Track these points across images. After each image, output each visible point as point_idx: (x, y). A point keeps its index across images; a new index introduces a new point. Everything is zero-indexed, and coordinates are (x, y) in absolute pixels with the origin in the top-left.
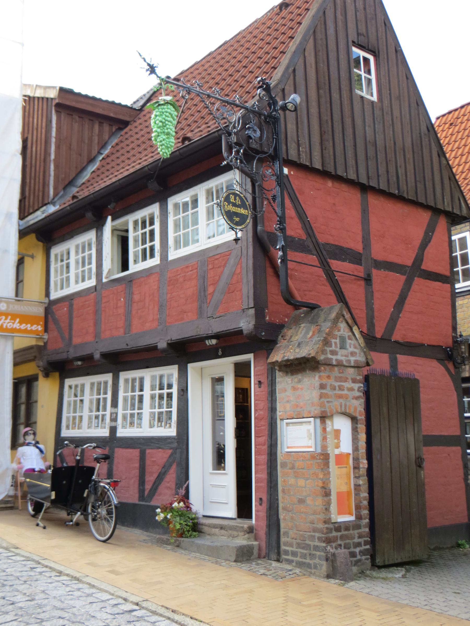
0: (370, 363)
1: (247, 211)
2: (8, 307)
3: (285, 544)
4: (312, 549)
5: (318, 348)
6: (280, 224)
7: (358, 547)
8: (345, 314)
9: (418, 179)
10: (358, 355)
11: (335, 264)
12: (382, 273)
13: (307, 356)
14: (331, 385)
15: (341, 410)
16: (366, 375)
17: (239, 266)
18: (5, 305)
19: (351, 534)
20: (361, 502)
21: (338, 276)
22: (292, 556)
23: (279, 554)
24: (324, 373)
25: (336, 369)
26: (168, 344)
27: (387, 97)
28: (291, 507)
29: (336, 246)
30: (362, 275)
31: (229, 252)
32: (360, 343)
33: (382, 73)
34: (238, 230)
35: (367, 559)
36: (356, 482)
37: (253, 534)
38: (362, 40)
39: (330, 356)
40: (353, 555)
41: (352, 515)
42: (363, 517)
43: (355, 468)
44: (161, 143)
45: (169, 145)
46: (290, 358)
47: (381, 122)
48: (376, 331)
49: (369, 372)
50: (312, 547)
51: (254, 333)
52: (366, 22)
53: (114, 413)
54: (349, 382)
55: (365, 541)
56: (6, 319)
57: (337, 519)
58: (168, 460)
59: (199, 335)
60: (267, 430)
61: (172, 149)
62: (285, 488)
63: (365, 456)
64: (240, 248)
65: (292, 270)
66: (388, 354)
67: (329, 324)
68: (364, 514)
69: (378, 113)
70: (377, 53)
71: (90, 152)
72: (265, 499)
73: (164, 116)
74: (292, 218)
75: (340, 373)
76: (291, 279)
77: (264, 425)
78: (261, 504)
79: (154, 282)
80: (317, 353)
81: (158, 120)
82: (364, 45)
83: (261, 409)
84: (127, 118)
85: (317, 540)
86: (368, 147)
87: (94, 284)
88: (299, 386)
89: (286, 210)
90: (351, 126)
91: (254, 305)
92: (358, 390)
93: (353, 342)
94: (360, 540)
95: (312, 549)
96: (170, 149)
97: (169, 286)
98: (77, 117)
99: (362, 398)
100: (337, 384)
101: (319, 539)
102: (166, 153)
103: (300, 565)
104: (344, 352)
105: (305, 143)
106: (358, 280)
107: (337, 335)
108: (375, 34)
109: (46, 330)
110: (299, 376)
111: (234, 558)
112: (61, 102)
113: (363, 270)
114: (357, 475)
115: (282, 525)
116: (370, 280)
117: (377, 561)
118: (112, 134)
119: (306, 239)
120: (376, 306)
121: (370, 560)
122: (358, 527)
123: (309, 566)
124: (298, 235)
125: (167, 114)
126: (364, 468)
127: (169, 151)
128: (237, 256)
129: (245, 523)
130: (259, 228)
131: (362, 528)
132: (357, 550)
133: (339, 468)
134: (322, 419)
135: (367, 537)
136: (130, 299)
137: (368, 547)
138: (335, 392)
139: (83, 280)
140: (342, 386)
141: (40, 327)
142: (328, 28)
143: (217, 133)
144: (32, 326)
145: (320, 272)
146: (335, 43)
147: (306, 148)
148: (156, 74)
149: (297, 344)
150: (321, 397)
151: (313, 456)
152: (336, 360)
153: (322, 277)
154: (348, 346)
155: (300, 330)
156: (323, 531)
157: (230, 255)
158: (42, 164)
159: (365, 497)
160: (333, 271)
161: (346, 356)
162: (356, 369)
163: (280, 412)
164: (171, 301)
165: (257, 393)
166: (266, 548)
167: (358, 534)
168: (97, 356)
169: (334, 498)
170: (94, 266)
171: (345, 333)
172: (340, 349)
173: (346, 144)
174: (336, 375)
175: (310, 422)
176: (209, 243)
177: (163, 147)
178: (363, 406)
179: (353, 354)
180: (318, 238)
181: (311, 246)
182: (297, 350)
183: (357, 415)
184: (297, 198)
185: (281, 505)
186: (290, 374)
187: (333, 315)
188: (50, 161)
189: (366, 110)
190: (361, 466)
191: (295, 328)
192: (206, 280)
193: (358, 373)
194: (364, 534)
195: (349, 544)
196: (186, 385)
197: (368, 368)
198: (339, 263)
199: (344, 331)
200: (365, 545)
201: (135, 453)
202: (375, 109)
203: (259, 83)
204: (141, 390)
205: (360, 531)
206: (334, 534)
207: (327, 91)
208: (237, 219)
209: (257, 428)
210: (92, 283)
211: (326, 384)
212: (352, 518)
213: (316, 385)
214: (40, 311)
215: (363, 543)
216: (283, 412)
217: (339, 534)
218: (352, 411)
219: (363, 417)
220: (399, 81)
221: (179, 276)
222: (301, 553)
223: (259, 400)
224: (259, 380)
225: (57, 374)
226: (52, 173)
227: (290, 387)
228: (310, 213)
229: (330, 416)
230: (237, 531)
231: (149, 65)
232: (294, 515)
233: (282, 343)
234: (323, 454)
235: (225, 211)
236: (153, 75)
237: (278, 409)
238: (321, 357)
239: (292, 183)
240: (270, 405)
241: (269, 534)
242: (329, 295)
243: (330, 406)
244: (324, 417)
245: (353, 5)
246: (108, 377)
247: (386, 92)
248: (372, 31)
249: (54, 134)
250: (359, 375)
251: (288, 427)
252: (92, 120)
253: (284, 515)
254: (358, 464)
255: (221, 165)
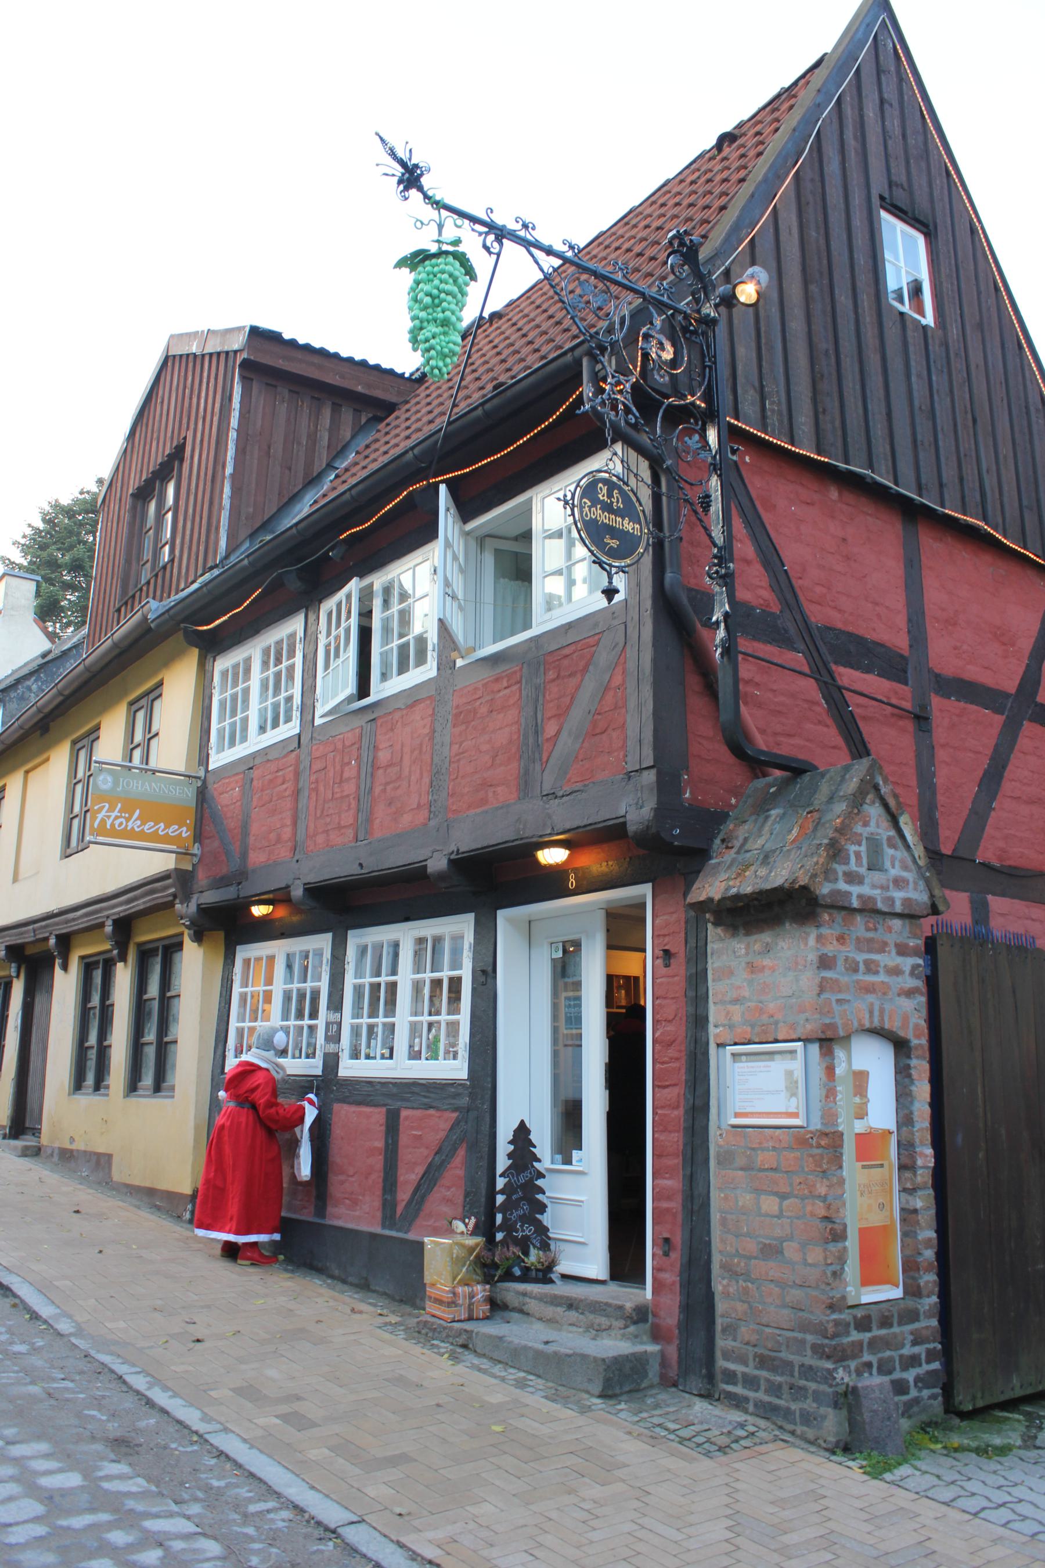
0: (941, 908)
1: (637, 526)
2: (116, 783)
3: (727, 1356)
4: (796, 1374)
5: (817, 863)
6: (719, 565)
7: (913, 1367)
8: (881, 783)
9: (1025, 502)
10: (911, 885)
11: (847, 676)
12: (953, 705)
13: (787, 885)
14: (847, 959)
15: (871, 1022)
16: (927, 938)
17: (619, 669)
18: (109, 779)
19: (895, 1335)
20: (920, 1254)
21: (855, 704)
22: (744, 1387)
23: (710, 1377)
24: (831, 928)
25: (859, 918)
26: (451, 862)
27: (956, 321)
28: (742, 1264)
29: (850, 635)
30: (907, 705)
31: (596, 638)
32: (917, 856)
33: (944, 270)
34: (614, 570)
35: (933, 1397)
36: (907, 1202)
37: (648, 1326)
38: (901, 198)
39: (842, 886)
40: (900, 1387)
41: (897, 1286)
42: (925, 1292)
43: (902, 1167)
44: (427, 345)
45: (446, 350)
46: (742, 892)
47: (945, 370)
48: (941, 839)
49: (935, 932)
50: (797, 1369)
51: (653, 830)
52: (907, 162)
53: (333, 1023)
54: (889, 952)
55: (928, 1351)
56: (111, 809)
57: (858, 1295)
58: (447, 1136)
59: (522, 839)
60: (683, 1071)
61: (455, 359)
62: (729, 1216)
63: (929, 1137)
64: (623, 626)
65: (747, 682)
66: (968, 894)
67: (840, 807)
68: (927, 1282)
69: (935, 348)
70: (931, 227)
71: (309, 464)
72: (678, 1239)
73: (436, 282)
74: (748, 562)
75: (868, 929)
76: (746, 704)
77: (677, 1059)
78: (666, 1254)
79: (422, 719)
80: (814, 876)
81: (422, 290)
82: (904, 208)
83: (671, 1018)
84: (393, 398)
85: (809, 1352)
86: (918, 420)
87: (297, 731)
88: (767, 962)
89: (734, 542)
90: (880, 370)
91: (655, 761)
92: (912, 974)
93: (901, 854)
94: (916, 1350)
95: (796, 1374)
96: (448, 360)
97: (454, 726)
98: (286, 393)
99: (921, 994)
100: (861, 957)
101: (816, 1349)
102: (440, 370)
103: (766, 1411)
104: (877, 877)
105: (777, 392)
106: (901, 717)
107: (861, 835)
108: (926, 189)
109: (199, 836)
110: (766, 937)
111: (597, 1389)
112: (252, 358)
113: (910, 695)
114: (909, 1185)
115: (720, 1306)
116: (927, 719)
117: (958, 1398)
118: (359, 430)
119: (781, 612)
120: (940, 781)
121: (940, 1398)
122: (912, 1316)
123: (787, 1414)
124: (762, 602)
125: (445, 276)
126: (927, 1167)
127: (446, 366)
128: (615, 647)
129: (627, 1296)
130: (669, 576)
131: (922, 1317)
132: (910, 1375)
133: (864, 1167)
134: (825, 1044)
135: (934, 1342)
136: (370, 760)
137: (936, 1365)
138: (855, 977)
139: (275, 724)
140: (873, 961)
141: (184, 829)
142: (825, 160)
143: (569, 355)
144: (167, 827)
145: (810, 687)
146: (841, 190)
147: (779, 403)
148: (420, 189)
149: (761, 857)
150: (822, 989)
151: (801, 1138)
152: (860, 897)
153: (818, 704)
154: (887, 864)
155: (769, 823)
156: (826, 1329)
157: (597, 644)
158: (209, 484)
159: (930, 1240)
160: (839, 688)
161: (882, 887)
162: (907, 921)
163: (716, 1026)
164: (459, 760)
165: (658, 981)
166: (679, 1363)
167: (912, 1333)
168: (297, 892)
169: (852, 1243)
170: (297, 691)
171: (880, 831)
172: (869, 869)
173: (870, 407)
174: (859, 934)
175: (793, 1052)
176: (550, 620)
177: (433, 353)
178: (924, 1012)
179: (899, 883)
180: (808, 613)
181: (793, 631)
182: (762, 872)
183: (909, 1034)
184: (760, 518)
185: (716, 1259)
186: (742, 931)
187: (852, 785)
188: (224, 477)
189: (910, 340)
190: (920, 1162)
191: (756, 821)
192: (540, 707)
193: (910, 932)
194: (925, 1333)
195: (891, 1359)
196: (491, 960)
197: (932, 919)
198: (857, 674)
199: (878, 827)
200: (928, 1362)
201: (377, 1116)
202: (930, 341)
203: (671, 243)
204: (394, 972)
205: (916, 1325)
206: (855, 1336)
207: (826, 289)
208: (614, 543)
209: (658, 1066)
210: (289, 729)
211: (835, 957)
212: (896, 1293)
213: (809, 959)
214: (188, 794)
215: (923, 1357)
216: (724, 1026)
217: (866, 1336)
218: (893, 1024)
219: (924, 1041)
220: (979, 293)
221: (478, 703)
222: (768, 1380)
223: (665, 998)
224: (666, 948)
225: (221, 935)
226: (226, 502)
227: (743, 964)
228: (792, 553)
229: (843, 1037)
230: (607, 1316)
231: (402, 163)
232: (750, 1285)
233: (722, 858)
234: (826, 1134)
235: (585, 523)
236: (413, 193)
237: (711, 1019)
238: (824, 889)
239: (746, 481)
240: (691, 1010)
241: (686, 1326)
242: (834, 747)
243: (845, 1011)
244: (830, 1040)
245: (880, 123)
246: (323, 942)
247: (952, 312)
248: (920, 182)
249: (234, 422)
250: (915, 936)
251: (737, 1065)
252: (318, 399)
253: (725, 1282)
254: (913, 1158)
255: (578, 412)
